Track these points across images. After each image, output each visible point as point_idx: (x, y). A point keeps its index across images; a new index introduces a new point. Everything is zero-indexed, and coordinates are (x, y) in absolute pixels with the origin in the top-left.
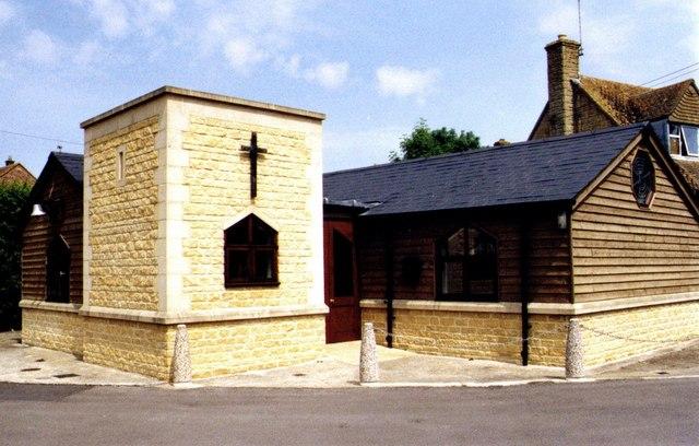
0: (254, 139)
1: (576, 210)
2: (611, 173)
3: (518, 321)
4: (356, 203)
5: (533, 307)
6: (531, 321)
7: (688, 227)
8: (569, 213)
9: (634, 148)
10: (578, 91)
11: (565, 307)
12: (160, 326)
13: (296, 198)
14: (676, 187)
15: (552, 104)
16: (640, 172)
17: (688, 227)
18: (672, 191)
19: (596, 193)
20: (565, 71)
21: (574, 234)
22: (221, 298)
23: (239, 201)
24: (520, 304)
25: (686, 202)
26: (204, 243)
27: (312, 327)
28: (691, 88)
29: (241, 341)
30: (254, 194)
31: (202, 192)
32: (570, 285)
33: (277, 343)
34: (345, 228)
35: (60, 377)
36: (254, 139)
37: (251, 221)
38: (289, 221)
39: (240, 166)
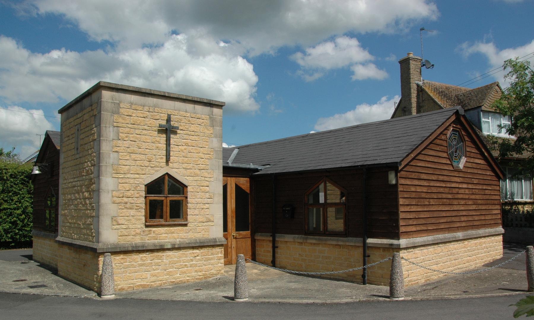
0: (169, 120)
1: (401, 170)
2: (431, 143)
3: (361, 250)
4: (252, 166)
5: (370, 241)
6: (368, 252)
7: (491, 182)
8: (397, 171)
9: (450, 125)
10: (420, 90)
11: (395, 242)
12: (94, 250)
13: (201, 161)
14: (482, 154)
15: (421, 101)
16: (454, 143)
17: (491, 182)
18: (479, 156)
19: (418, 157)
20: (412, 77)
21: (400, 189)
22: (142, 233)
23: (157, 164)
24: (362, 239)
25: (490, 165)
26: (129, 193)
27: (212, 254)
28: (497, 87)
29: (158, 264)
30: (168, 161)
31: (128, 157)
32: (397, 227)
33: (186, 265)
34: (244, 182)
35: (31, 287)
36: (169, 120)
37: (167, 177)
38: (196, 178)
39: (158, 139)
